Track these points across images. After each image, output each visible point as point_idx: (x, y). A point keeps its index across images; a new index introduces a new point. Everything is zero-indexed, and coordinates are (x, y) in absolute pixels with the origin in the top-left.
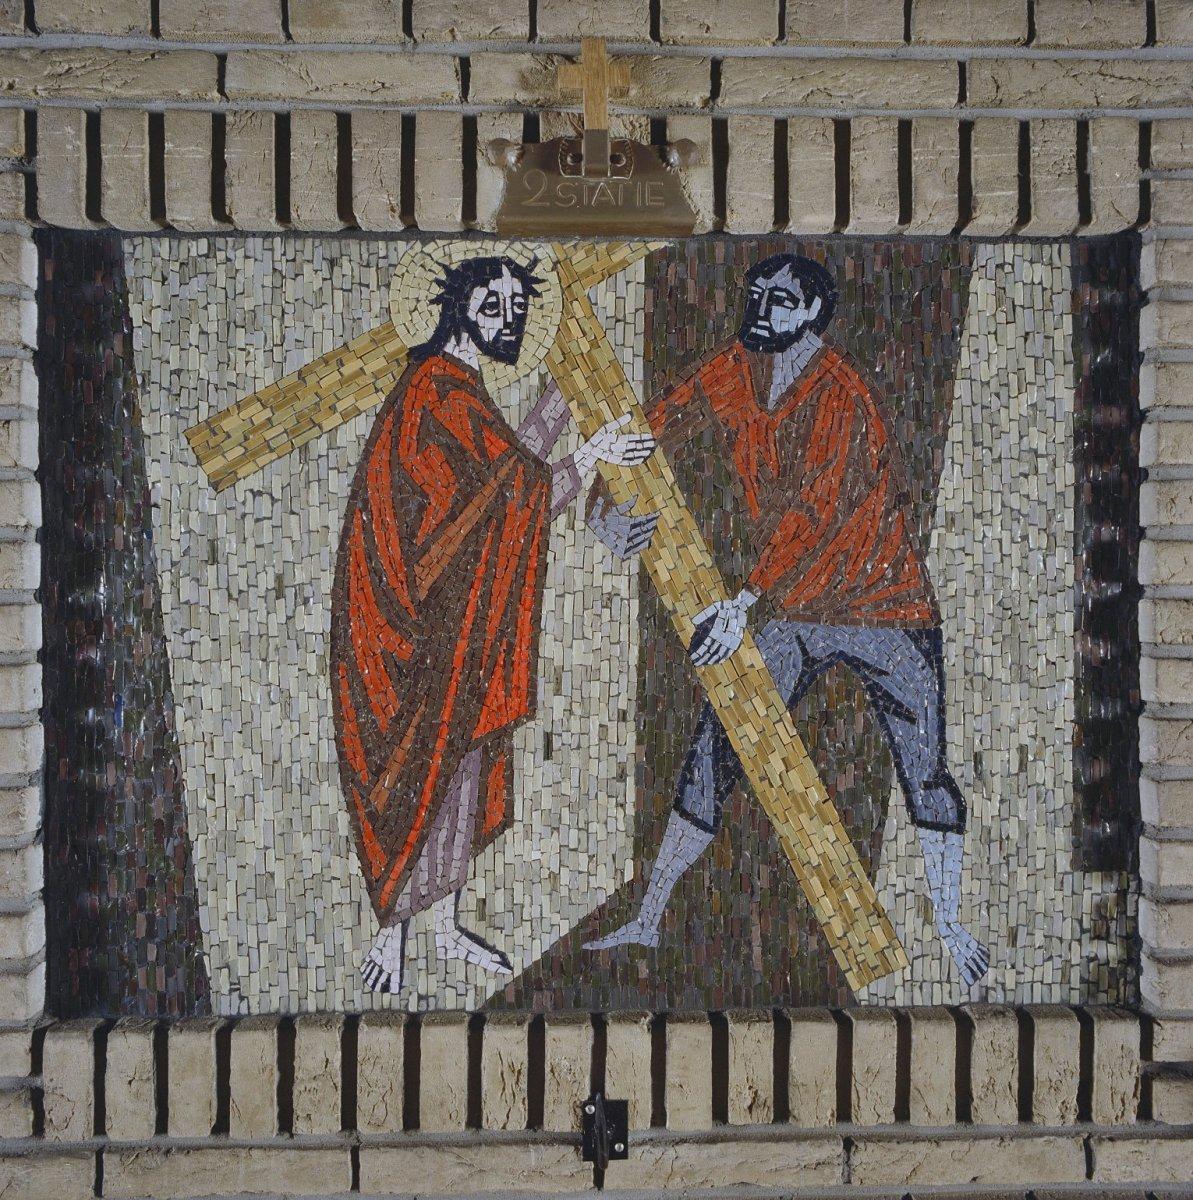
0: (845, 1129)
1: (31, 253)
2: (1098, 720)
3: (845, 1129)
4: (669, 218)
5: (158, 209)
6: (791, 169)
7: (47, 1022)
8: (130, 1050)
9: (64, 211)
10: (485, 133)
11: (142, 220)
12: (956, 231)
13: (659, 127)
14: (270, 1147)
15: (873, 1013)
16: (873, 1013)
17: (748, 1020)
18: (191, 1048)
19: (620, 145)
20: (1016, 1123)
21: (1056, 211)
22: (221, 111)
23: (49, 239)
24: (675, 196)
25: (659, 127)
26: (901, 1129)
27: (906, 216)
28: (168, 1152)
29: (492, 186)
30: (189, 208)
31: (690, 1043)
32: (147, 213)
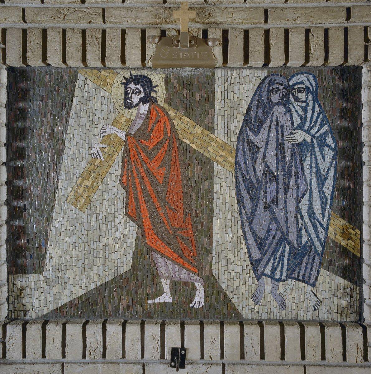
0: (303, 362)
1: (5, 73)
2: (19, 219)
3: (63, 360)
4: (209, 63)
5: (84, 60)
6: (344, 51)
7: (8, 321)
8: (212, 331)
9: (14, 60)
10: (149, 33)
11: (80, 64)
12: (285, 64)
13: (205, 32)
14: (237, 364)
15: (251, 322)
16: (251, 322)
17: (230, 324)
18: (232, 331)
19: (193, 38)
20: (239, 359)
21: (317, 60)
22: (309, 28)
23: (11, 70)
24: (212, 56)
25: (205, 32)
26: (344, 363)
27: (307, 60)
28: (89, 364)
29: (151, 48)
30: (93, 59)
31: (114, 330)
32: (41, 60)
